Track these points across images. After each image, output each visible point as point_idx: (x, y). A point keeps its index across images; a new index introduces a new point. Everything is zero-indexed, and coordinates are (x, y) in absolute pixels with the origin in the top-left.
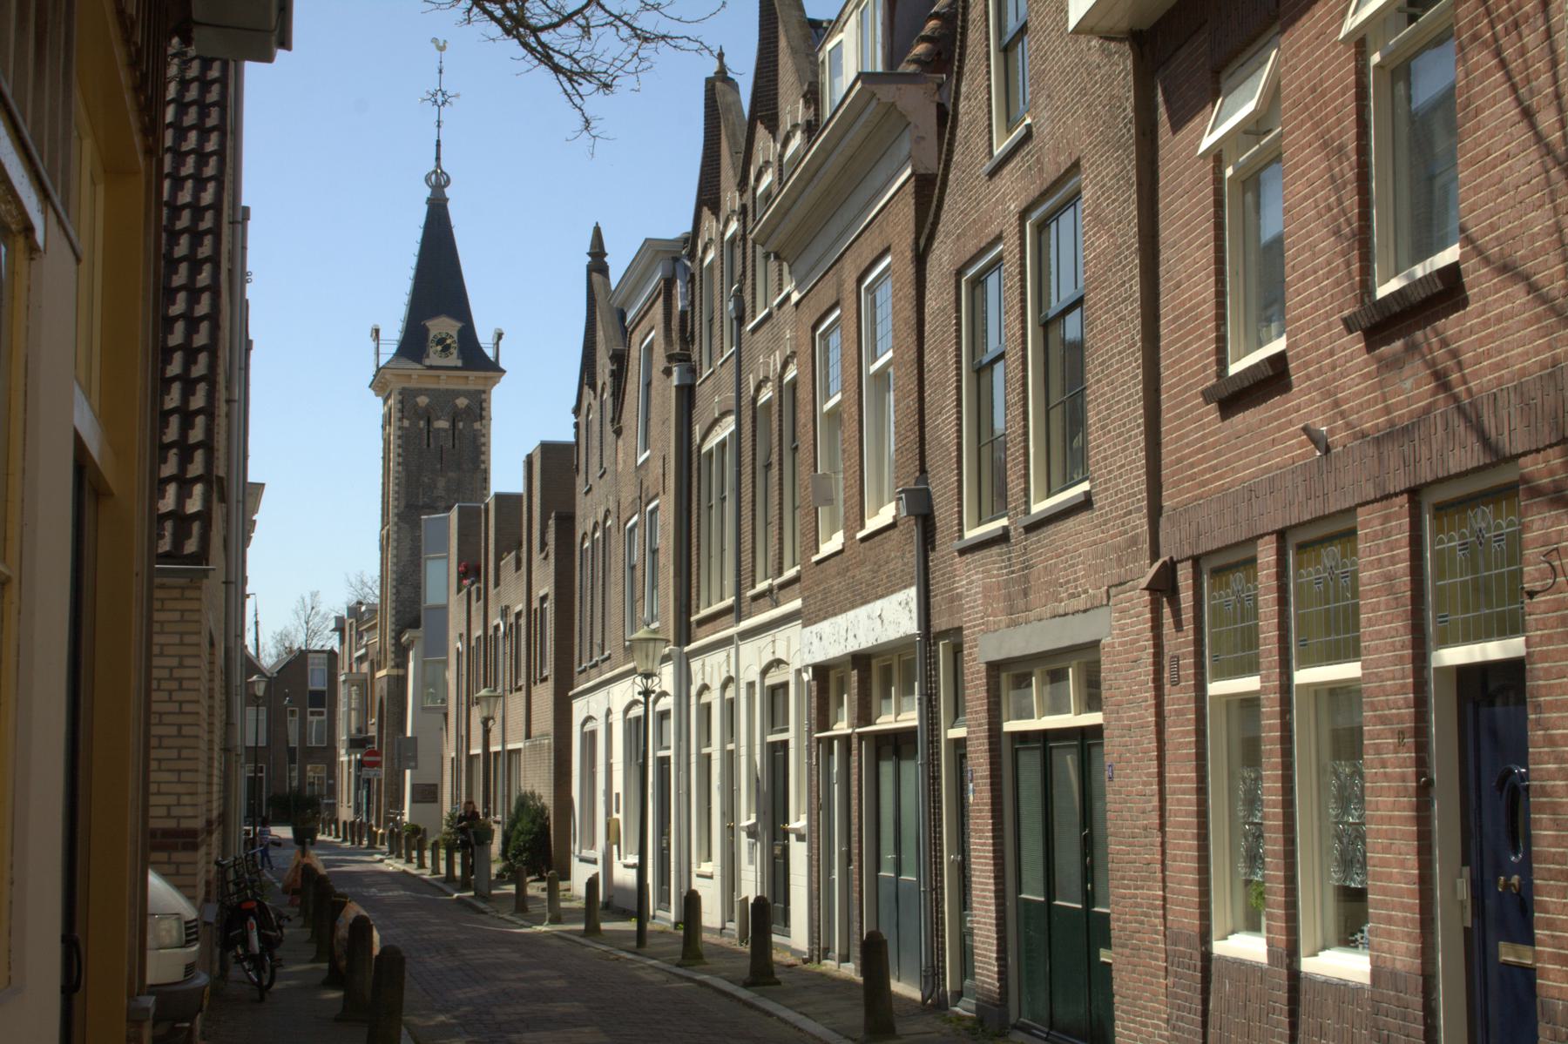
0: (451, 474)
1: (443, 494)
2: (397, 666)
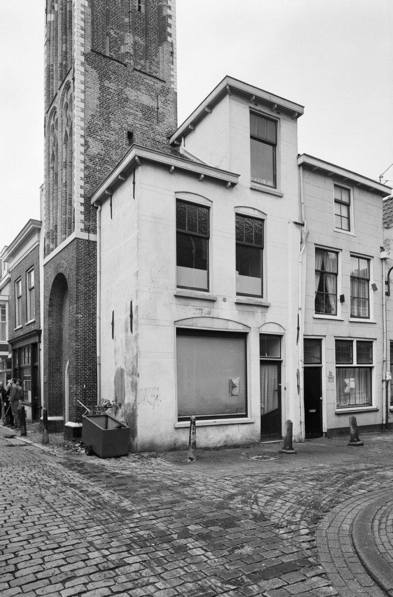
0: (137, 38)
1: (132, 51)
2: (87, 229)
